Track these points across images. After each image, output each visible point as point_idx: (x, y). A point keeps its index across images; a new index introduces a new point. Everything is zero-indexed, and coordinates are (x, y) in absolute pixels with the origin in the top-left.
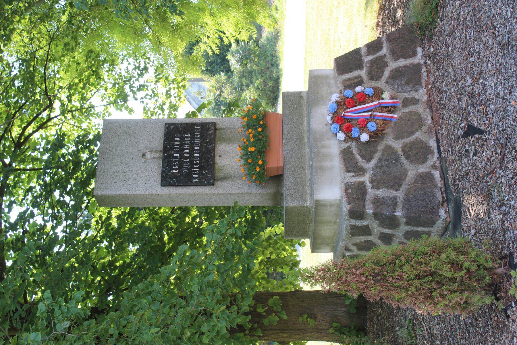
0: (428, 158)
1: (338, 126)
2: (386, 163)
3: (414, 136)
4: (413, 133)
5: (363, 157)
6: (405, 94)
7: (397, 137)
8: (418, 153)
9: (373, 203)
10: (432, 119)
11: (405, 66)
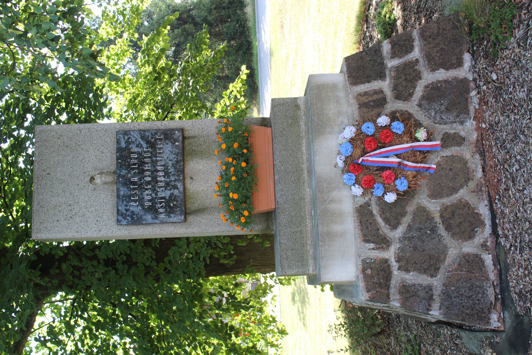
0: (477, 232)
1: (354, 178)
3: (457, 195)
4: (455, 190)
5: (387, 221)
6: (445, 126)
7: (434, 195)
8: (462, 221)
9: (401, 293)
10: (483, 171)
11: (446, 81)
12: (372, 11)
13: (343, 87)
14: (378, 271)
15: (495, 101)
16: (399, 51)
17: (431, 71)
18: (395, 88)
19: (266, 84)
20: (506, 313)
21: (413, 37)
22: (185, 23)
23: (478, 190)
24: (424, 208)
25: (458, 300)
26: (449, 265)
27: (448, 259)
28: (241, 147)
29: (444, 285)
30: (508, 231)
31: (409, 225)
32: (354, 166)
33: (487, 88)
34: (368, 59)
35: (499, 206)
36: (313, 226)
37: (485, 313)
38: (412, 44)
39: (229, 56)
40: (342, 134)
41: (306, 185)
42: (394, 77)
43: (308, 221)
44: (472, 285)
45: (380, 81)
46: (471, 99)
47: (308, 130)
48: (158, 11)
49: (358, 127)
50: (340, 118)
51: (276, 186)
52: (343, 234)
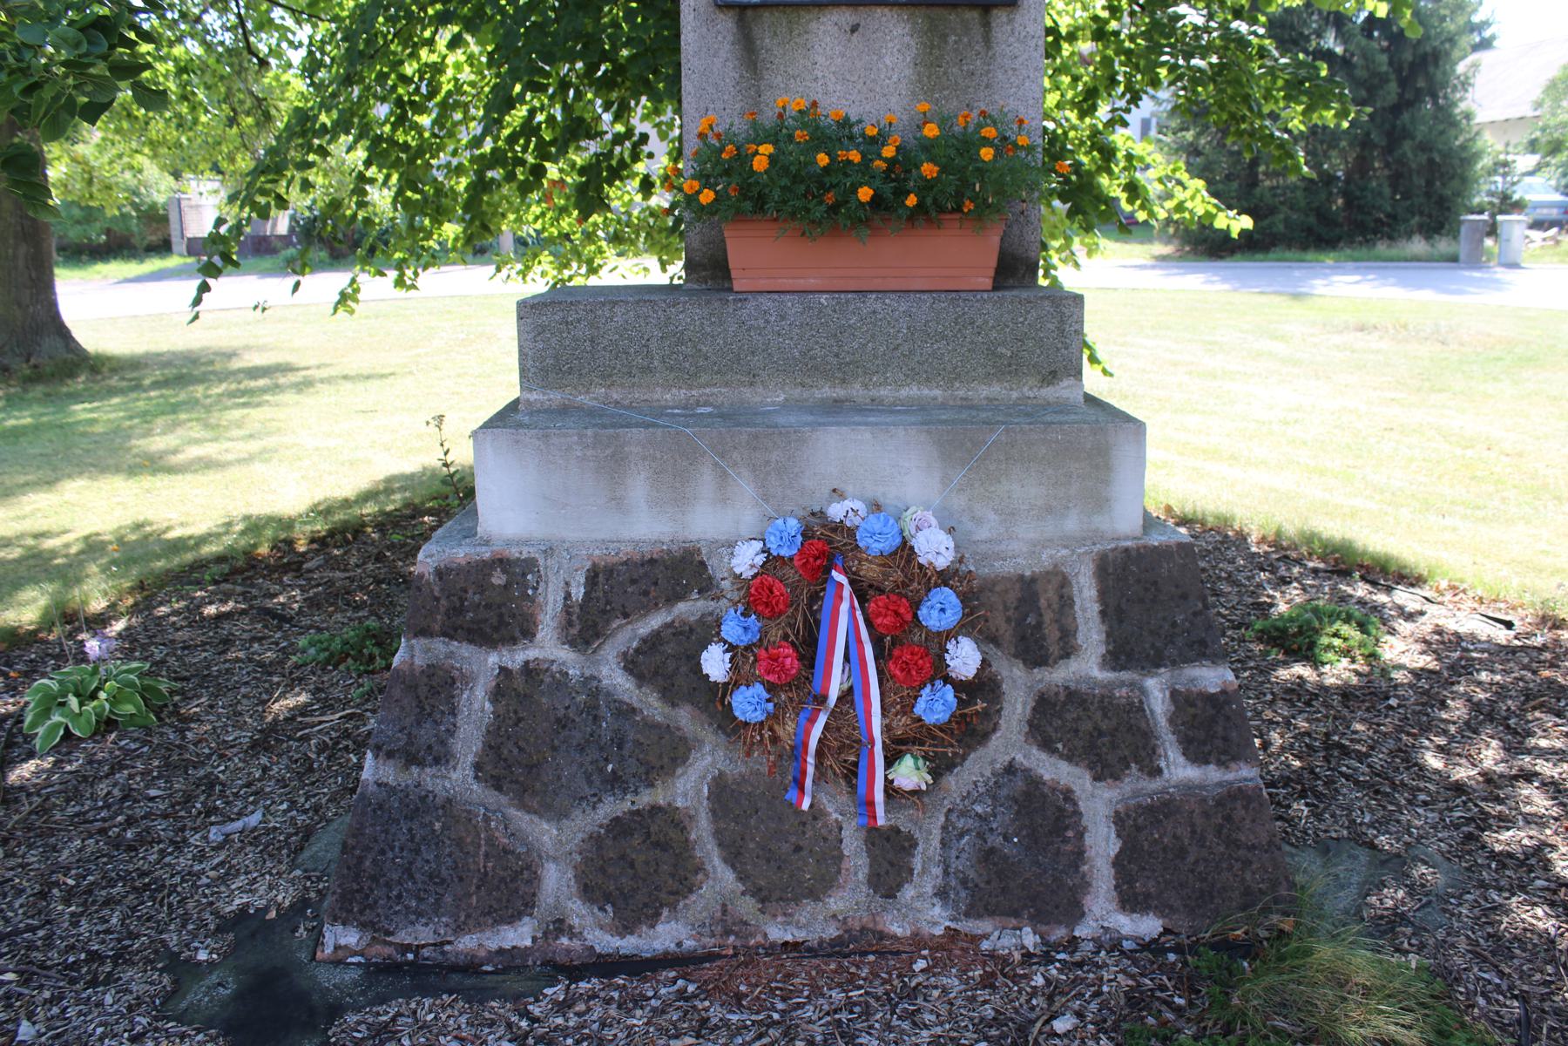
0: (602, 909)
1: (785, 552)
2: (607, 737)
3: (717, 861)
4: (733, 857)
5: (652, 643)
6: (936, 843)
7: (722, 793)
8: (634, 870)
9: (431, 670)
11: (1079, 855)
12: (1361, 590)
13: (1097, 530)
14: (499, 607)
15: (982, 1019)
16: (1195, 716)
17: (1116, 812)
18: (1074, 696)
19: (1225, 280)
20: (352, 975)
21: (1233, 765)
22: (1403, 83)
23: (727, 922)
24: (685, 760)
25: (403, 839)
26: (506, 822)
27: (527, 817)
28: (926, 186)
29: (449, 801)
30: (578, 1014)
31: (634, 710)
32: (822, 554)
33: (1035, 991)
34: (1179, 619)
35: (663, 991)
36: (661, 411)
37: (361, 912)
38: (1212, 759)
39: (1305, 189)
40: (934, 522)
41: (797, 392)
42: (1112, 697)
43: (682, 394)
44: (443, 881)
45: (1102, 650)
46: (1015, 929)
47: (971, 407)
48: (1442, 12)
49: (945, 577)
50: (992, 516)
51: (893, 296)
52: (618, 503)
